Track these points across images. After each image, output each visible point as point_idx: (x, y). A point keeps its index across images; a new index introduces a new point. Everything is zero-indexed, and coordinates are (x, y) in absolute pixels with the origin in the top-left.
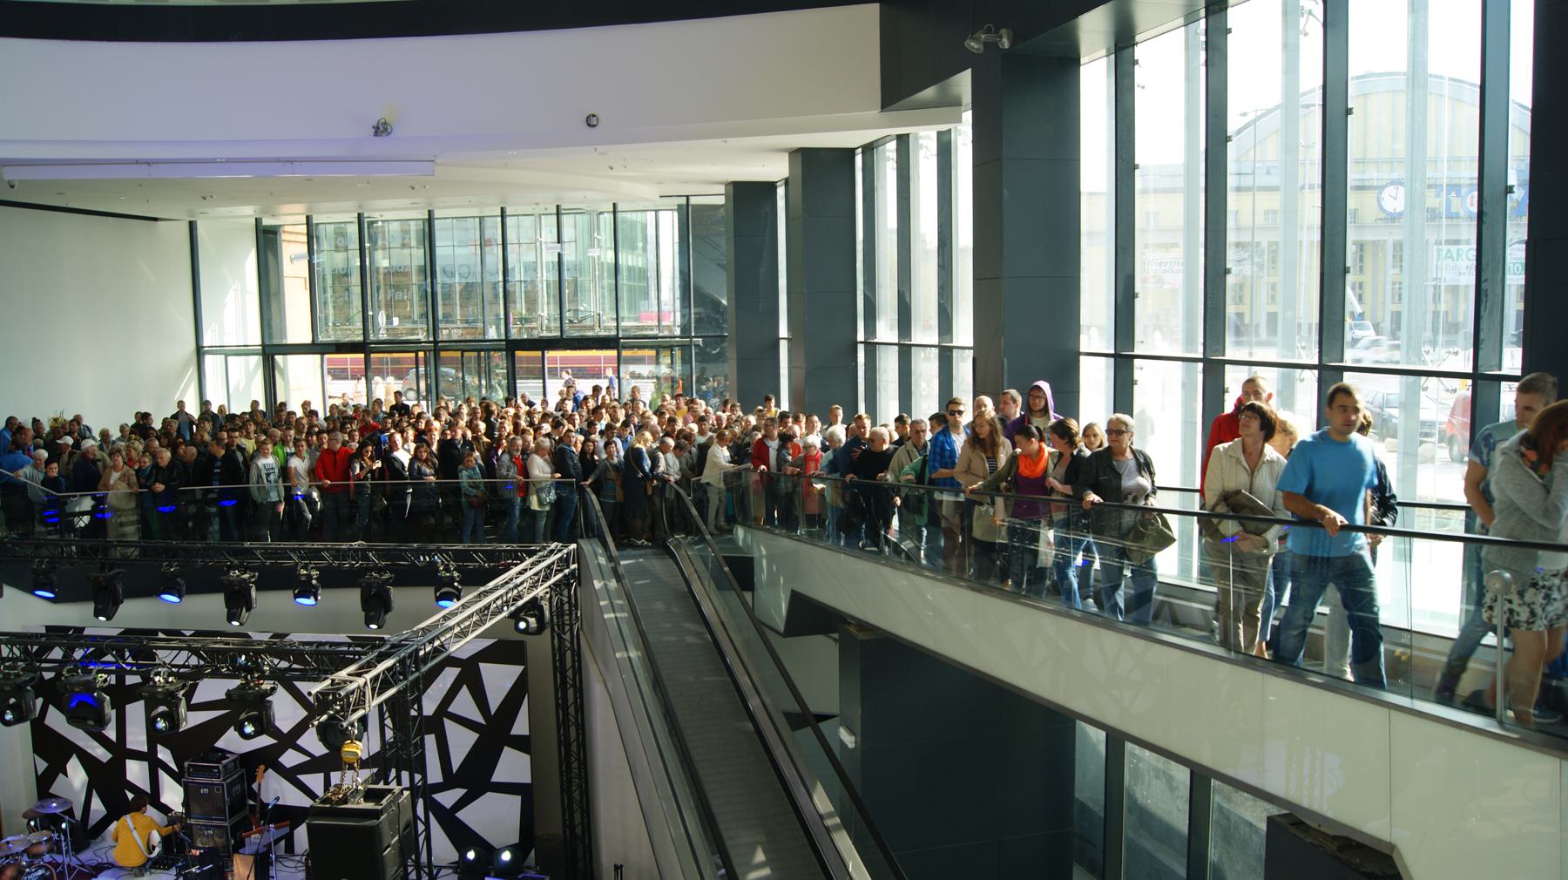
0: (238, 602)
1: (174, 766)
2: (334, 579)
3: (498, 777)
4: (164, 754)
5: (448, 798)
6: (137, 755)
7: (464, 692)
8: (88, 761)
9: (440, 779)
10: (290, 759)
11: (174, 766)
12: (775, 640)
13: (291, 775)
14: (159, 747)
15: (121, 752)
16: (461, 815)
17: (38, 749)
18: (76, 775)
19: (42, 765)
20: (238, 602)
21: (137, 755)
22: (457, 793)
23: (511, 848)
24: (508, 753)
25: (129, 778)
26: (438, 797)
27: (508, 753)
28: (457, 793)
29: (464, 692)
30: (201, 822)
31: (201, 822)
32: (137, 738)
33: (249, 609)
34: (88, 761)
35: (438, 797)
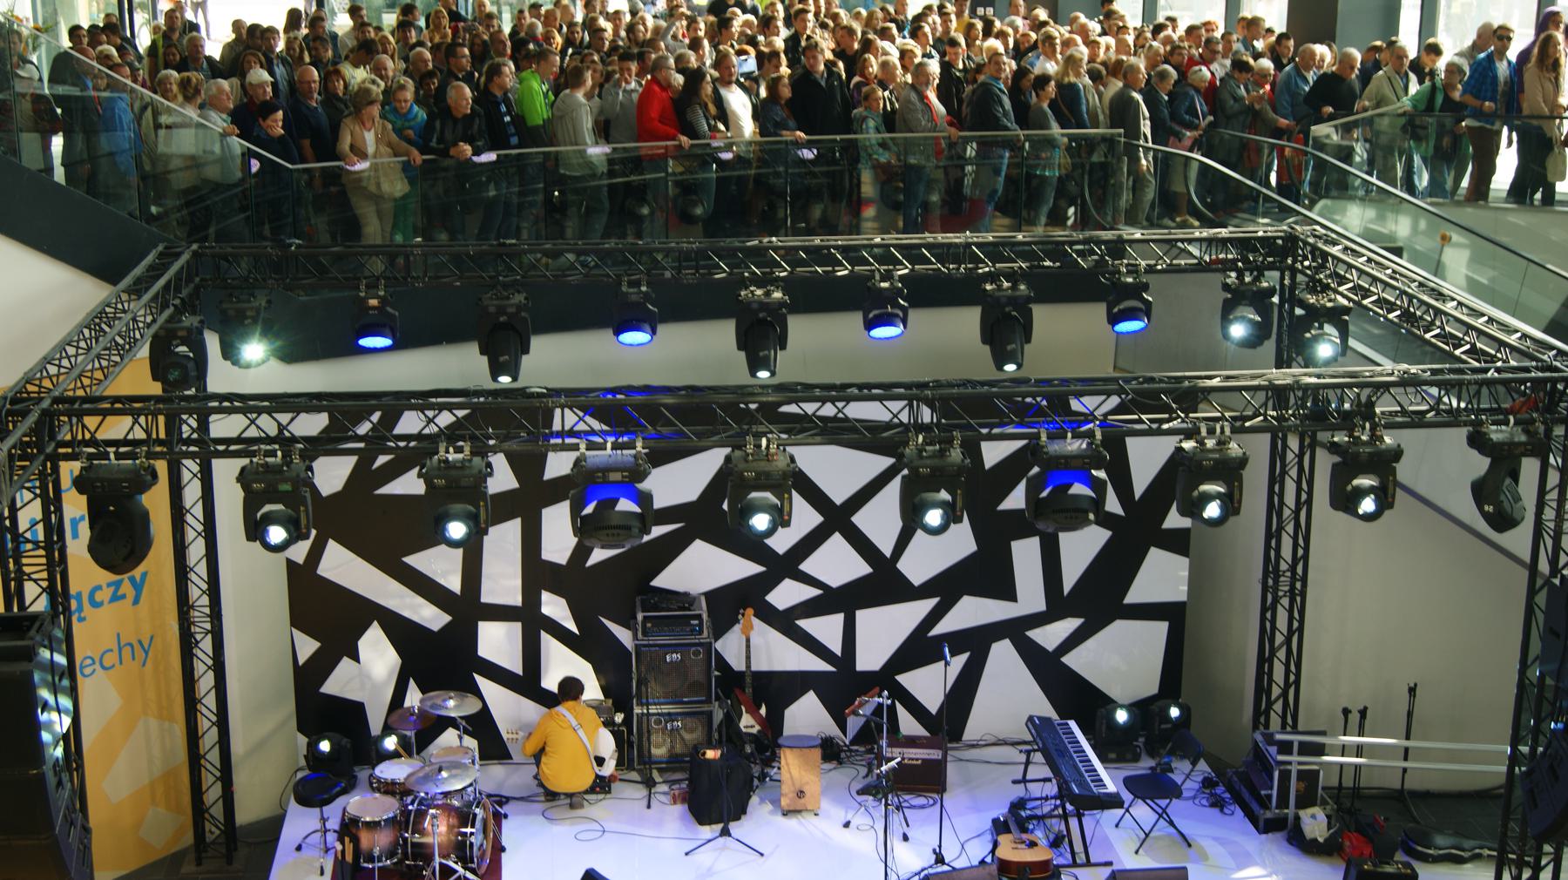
0: (760, 336)
1: (571, 626)
2: (930, 292)
3: (1134, 596)
4: (554, 607)
5: (1050, 636)
6: (500, 613)
7: (454, 583)
8: (401, 631)
9: (1040, 605)
10: (786, 594)
11: (571, 626)
12: (1177, 438)
13: (785, 622)
14: (546, 596)
15: (468, 608)
16: (1071, 660)
17: (301, 617)
18: (377, 658)
19: (307, 647)
20: (760, 336)
21: (500, 613)
22: (1068, 625)
23: (1130, 708)
24: (1156, 556)
25: (481, 653)
26: (1037, 635)
27: (1156, 556)
28: (1068, 625)
29: (454, 583)
30: (666, 709)
31: (666, 709)
32: (502, 581)
33: (783, 347)
34: (401, 631)
35: (1037, 635)
